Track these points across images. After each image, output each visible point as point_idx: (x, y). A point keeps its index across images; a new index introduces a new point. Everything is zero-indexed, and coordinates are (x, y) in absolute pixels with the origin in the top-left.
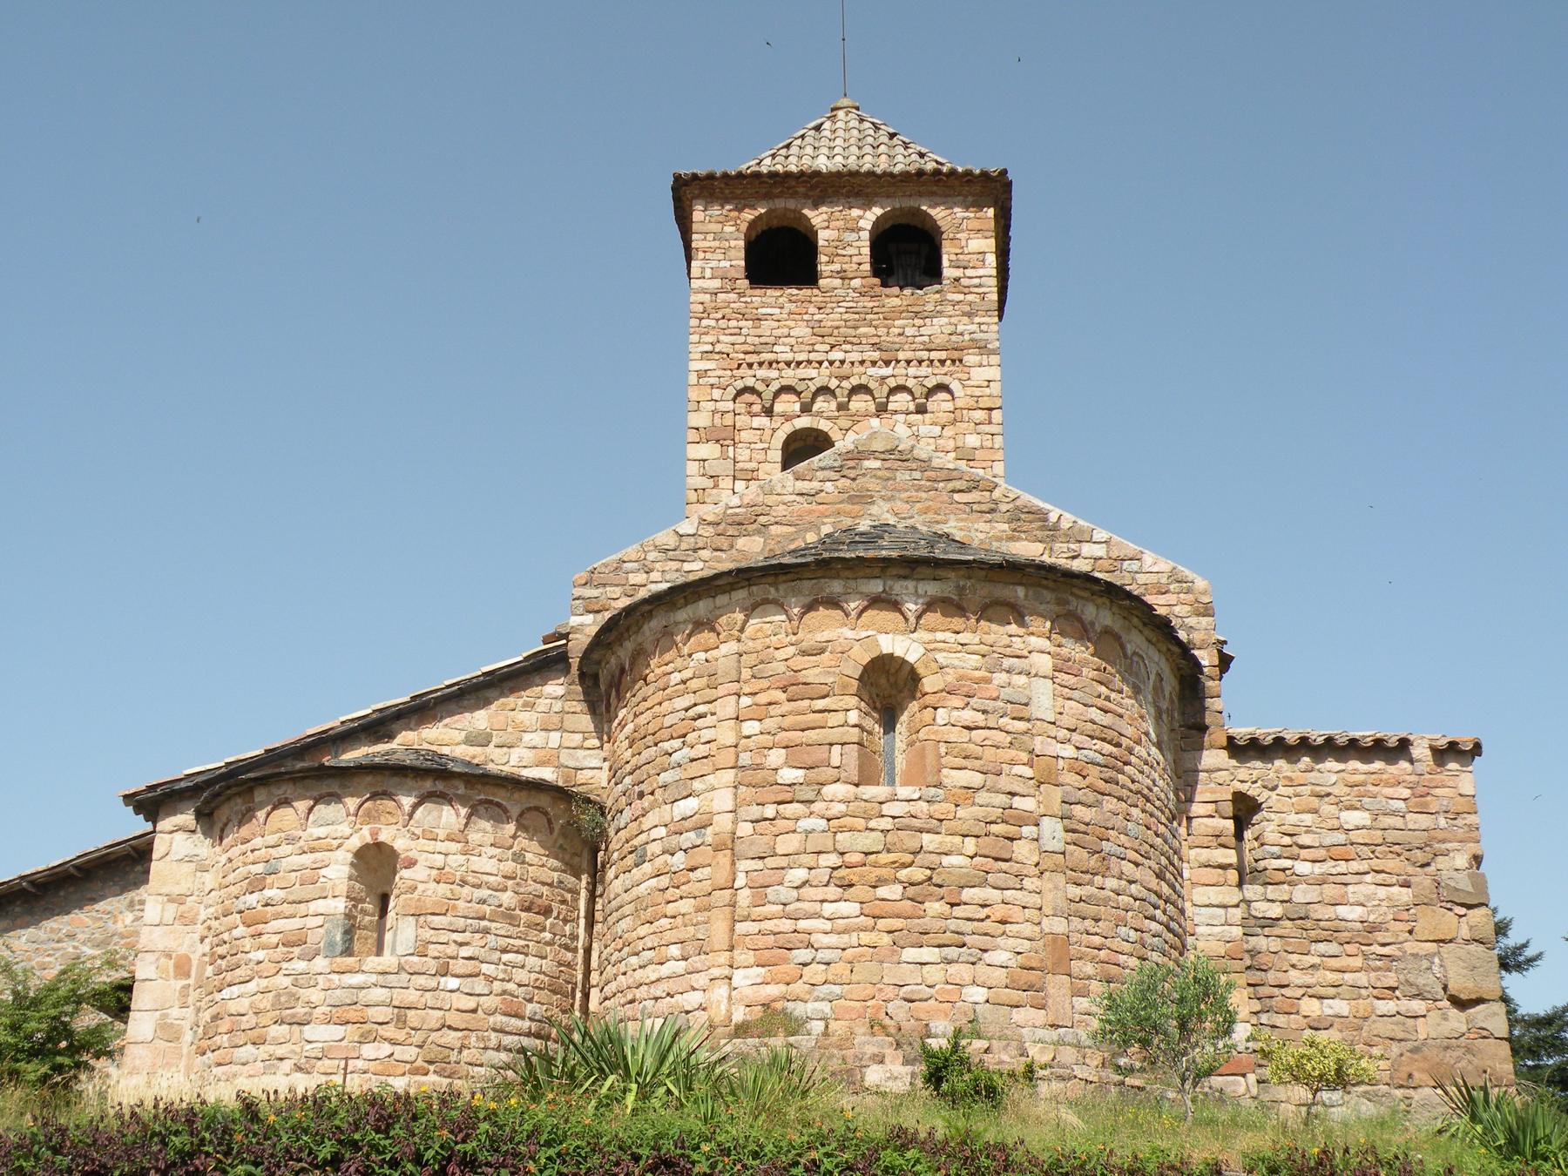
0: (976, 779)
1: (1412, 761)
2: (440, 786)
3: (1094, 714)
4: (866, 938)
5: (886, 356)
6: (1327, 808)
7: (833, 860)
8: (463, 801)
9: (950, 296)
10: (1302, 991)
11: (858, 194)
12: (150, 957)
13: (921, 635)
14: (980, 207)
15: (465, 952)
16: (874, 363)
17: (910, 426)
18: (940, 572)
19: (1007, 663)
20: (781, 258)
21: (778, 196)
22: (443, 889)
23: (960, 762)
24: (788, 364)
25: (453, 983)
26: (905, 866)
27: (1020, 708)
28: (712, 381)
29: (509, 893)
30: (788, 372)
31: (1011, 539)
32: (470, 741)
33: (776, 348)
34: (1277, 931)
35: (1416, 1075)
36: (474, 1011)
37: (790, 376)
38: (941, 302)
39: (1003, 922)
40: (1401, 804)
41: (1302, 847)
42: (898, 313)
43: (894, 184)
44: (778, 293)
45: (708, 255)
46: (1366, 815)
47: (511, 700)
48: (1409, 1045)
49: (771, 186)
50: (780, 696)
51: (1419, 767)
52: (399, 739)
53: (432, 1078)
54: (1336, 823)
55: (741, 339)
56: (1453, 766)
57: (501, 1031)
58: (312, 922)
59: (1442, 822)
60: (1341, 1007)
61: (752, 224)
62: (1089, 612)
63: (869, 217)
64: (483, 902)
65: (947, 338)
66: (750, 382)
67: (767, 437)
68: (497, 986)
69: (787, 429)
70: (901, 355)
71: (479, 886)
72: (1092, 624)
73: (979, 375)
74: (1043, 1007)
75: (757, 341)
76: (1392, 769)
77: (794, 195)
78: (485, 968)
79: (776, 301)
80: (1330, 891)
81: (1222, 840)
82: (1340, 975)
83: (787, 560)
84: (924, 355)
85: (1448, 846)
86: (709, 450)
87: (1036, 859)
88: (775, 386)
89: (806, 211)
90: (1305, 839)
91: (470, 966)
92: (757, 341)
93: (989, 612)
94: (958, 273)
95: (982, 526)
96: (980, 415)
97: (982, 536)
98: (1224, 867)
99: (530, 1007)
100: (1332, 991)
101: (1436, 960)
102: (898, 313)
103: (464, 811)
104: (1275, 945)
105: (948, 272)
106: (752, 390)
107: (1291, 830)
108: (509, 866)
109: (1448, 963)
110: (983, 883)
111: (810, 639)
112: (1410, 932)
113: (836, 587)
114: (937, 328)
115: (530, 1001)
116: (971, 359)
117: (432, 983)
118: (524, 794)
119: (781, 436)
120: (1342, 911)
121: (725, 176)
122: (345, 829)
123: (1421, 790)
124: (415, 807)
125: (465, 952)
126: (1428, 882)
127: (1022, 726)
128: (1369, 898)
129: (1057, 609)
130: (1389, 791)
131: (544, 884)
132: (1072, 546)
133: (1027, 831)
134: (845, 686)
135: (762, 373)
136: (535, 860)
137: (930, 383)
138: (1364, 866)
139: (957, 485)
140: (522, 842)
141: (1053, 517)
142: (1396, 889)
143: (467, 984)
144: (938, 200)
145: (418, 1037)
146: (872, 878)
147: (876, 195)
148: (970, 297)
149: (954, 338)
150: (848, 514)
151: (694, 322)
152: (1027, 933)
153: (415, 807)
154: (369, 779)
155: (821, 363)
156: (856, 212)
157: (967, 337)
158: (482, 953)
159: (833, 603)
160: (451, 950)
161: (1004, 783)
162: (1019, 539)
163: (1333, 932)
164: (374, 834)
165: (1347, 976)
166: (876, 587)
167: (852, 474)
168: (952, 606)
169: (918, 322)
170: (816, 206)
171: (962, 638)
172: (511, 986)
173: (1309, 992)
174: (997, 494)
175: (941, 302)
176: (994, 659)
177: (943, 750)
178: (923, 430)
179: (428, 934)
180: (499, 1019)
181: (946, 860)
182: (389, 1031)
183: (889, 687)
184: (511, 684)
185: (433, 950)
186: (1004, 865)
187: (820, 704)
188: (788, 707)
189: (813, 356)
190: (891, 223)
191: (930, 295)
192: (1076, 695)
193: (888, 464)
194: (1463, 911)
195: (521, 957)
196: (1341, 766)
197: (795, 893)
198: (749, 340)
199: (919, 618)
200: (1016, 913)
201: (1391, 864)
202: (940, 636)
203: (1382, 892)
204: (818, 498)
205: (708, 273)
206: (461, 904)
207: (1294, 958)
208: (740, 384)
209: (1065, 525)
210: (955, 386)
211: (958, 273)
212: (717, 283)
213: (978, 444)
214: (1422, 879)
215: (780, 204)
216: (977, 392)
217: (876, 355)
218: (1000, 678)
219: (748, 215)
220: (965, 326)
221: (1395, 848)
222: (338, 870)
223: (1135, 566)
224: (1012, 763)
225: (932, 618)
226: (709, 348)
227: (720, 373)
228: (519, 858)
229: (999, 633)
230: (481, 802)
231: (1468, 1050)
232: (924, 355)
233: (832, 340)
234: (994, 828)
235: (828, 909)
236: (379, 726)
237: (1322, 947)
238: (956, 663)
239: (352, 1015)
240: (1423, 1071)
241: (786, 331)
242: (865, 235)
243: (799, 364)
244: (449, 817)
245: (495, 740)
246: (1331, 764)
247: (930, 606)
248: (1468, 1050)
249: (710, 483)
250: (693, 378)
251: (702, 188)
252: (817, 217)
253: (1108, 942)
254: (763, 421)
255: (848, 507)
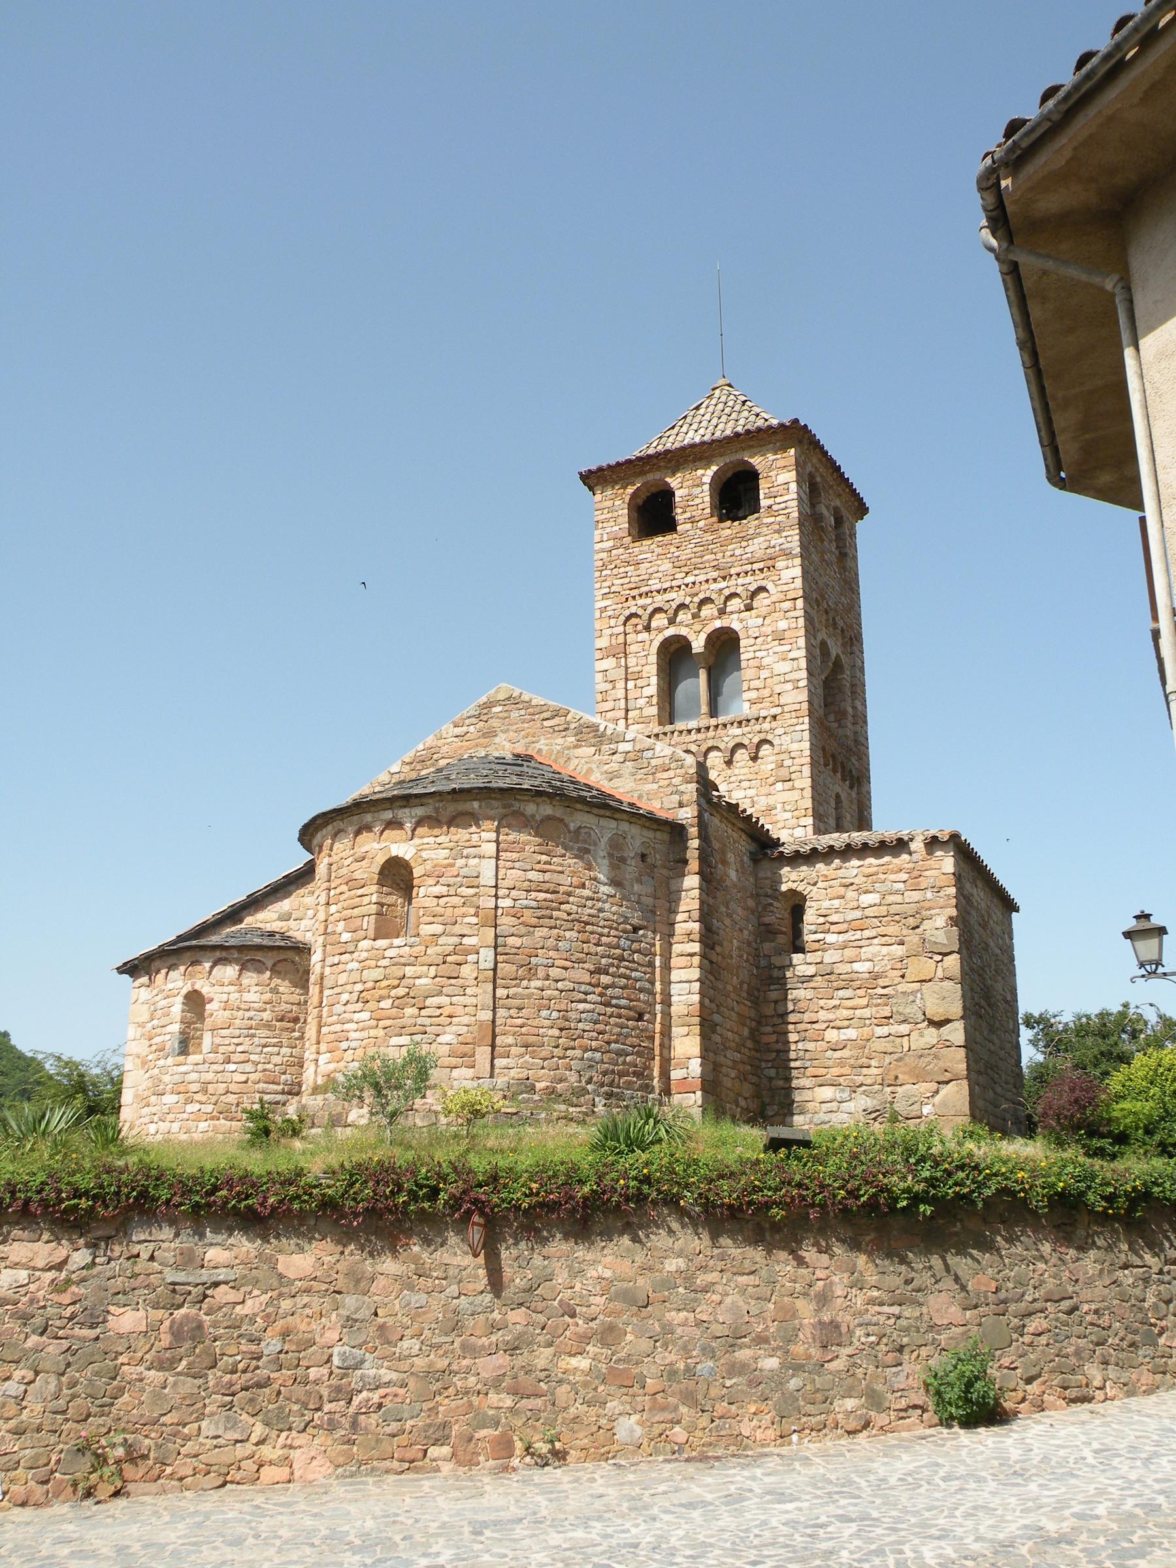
0: (438, 929)
1: (910, 854)
2: (224, 954)
3: (532, 875)
4: (373, 1033)
5: (722, 573)
6: (851, 894)
7: (359, 987)
8: (236, 961)
9: (766, 520)
10: (826, 1025)
11: (700, 459)
12: (130, 1058)
13: (416, 841)
14: (784, 449)
15: (240, 1049)
16: (715, 580)
17: (741, 621)
18: (424, 801)
19: (465, 852)
20: (654, 516)
21: (649, 471)
22: (227, 1013)
23: (431, 919)
24: (658, 592)
25: (232, 1067)
26: (395, 987)
27: (473, 881)
28: (609, 613)
29: (268, 1012)
30: (658, 598)
31: (576, 747)
32: (280, 919)
33: (650, 582)
34: (812, 984)
35: (900, 1076)
36: (246, 1082)
37: (659, 601)
38: (758, 527)
39: (451, 1017)
40: (901, 886)
41: (832, 924)
42: (730, 540)
43: (722, 447)
44: (650, 542)
45: (605, 525)
46: (878, 895)
47: (301, 891)
48: (896, 1056)
49: (642, 466)
50: (344, 888)
51: (915, 857)
52: (245, 921)
53: (222, 1121)
54: (855, 904)
55: (627, 580)
56: (939, 853)
57: (263, 1092)
58: (168, 1037)
59: (929, 895)
60: (851, 1033)
61: (634, 496)
62: (530, 808)
63: (707, 474)
64: (251, 1019)
65: (763, 551)
66: (633, 610)
67: (647, 647)
68: (260, 1067)
69: (660, 638)
70: (733, 571)
71: (248, 1010)
72: (533, 816)
73: (786, 575)
74: (473, 1067)
75: (637, 579)
76: (896, 861)
77: (659, 469)
78: (253, 1057)
79: (651, 547)
80: (849, 953)
81: (692, 937)
82: (852, 1011)
83: (374, 797)
84: (748, 567)
85: (932, 912)
86: (609, 663)
87: (475, 975)
88: (650, 609)
89: (668, 479)
90: (834, 918)
91: (243, 1057)
92: (637, 579)
93: (458, 821)
94: (770, 502)
95: (560, 741)
96: (787, 605)
97: (559, 748)
98: (692, 955)
99: (283, 1077)
100: (846, 1023)
101: (919, 995)
102: (730, 540)
103: (237, 968)
104: (809, 994)
105: (764, 503)
106: (635, 615)
107: (823, 912)
108: (267, 996)
109: (926, 996)
110: (440, 994)
111: (360, 851)
112: (903, 976)
113: (368, 818)
114: (757, 546)
115: (284, 1073)
116: (780, 564)
117: (221, 1068)
118: (275, 952)
119: (656, 644)
120: (857, 966)
121: (609, 466)
122: (180, 984)
123: (916, 873)
124: (212, 968)
125: (240, 1049)
126: (916, 939)
127: (472, 891)
128: (875, 955)
129: (504, 811)
130: (893, 877)
131: (293, 1004)
132: (612, 746)
133: (472, 958)
134: (371, 880)
135: (641, 602)
136: (287, 991)
137: (752, 588)
138: (873, 933)
139: (545, 715)
140: (276, 981)
141: (602, 728)
142: (895, 946)
143: (241, 1067)
144: (755, 450)
145: (214, 1099)
146: (377, 996)
147: (713, 456)
148: (779, 519)
149: (768, 551)
150: (481, 745)
151: (597, 574)
152: (466, 1022)
153: (212, 968)
154: (189, 954)
155: (679, 587)
156: (700, 472)
157: (777, 548)
158: (251, 1049)
159: (369, 828)
160: (231, 1048)
161: (457, 929)
162: (581, 746)
163: (849, 982)
164: (193, 985)
165: (857, 1012)
166: (388, 815)
167: (484, 718)
168: (431, 821)
169: (744, 544)
170: (673, 474)
171: (439, 840)
172: (270, 1066)
173: (830, 1025)
174: (569, 718)
175: (758, 527)
176: (457, 851)
177: (421, 914)
178: (751, 623)
179: (218, 1040)
180: (261, 1086)
181: (418, 982)
182: (198, 1097)
183: (397, 876)
184: (301, 881)
185: (222, 1049)
186: (453, 981)
187: (360, 892)
188: (348, 894)
189: (675, 583)
190: (729, 474)
191: (751, 522)
192: (517, 865)
193: (506, 708)
194: (939, 958)
195: (276, 1049)
196: (861, 863)
197: (343, 1008)
198: (632, 579)
199: (414, 830)
200: (459, 1010)
201: (892, 929)
202: (426, 840)
203: (885, 950)
204: (466, 738)
205: (605, 538)
206: (237, 1021)
207: (822, 1002)
208: (627, 613)
209: (609, 732)
210: (770, 586)
211: (770, 502)
212: (611, 543)
213: (786, 627)
214: (913, 939)
215: (650, 477)
216: (785, 588)
217: (715, 574)
218: (460, 862)
219: (630, 490)
220: (776, 540)
221: (897, 917)
222: (177, 1008)
223: (649, 754)
224: (464, 916)
225: (420, 830)
226: (607, 590)
227: (614, 607)
228: (275, 991)
229: (460, 834)
230: (248, 961)
231: (936, 1057)
232: (748, 567)
233: (686, 569)
234: (449, 959)
235: (356, 1016)
236: (234, 914)
237: (841, 993)
238: (434, 856)
239: (182, 1089)
240: (905, 1073)
241: (655, 569)
242: (706, 487)
243: (665, 590)
244: (230, 971)
245: (294, 916)
246: (855, 862)
247: (419, 823)
248: (936, 1057)
249: (609, 686)
250: (597, 614)
251: (599, 477)
252: (673, 482)
253: (529, 1022)
254: (644, 636)
255: (482, 740)
